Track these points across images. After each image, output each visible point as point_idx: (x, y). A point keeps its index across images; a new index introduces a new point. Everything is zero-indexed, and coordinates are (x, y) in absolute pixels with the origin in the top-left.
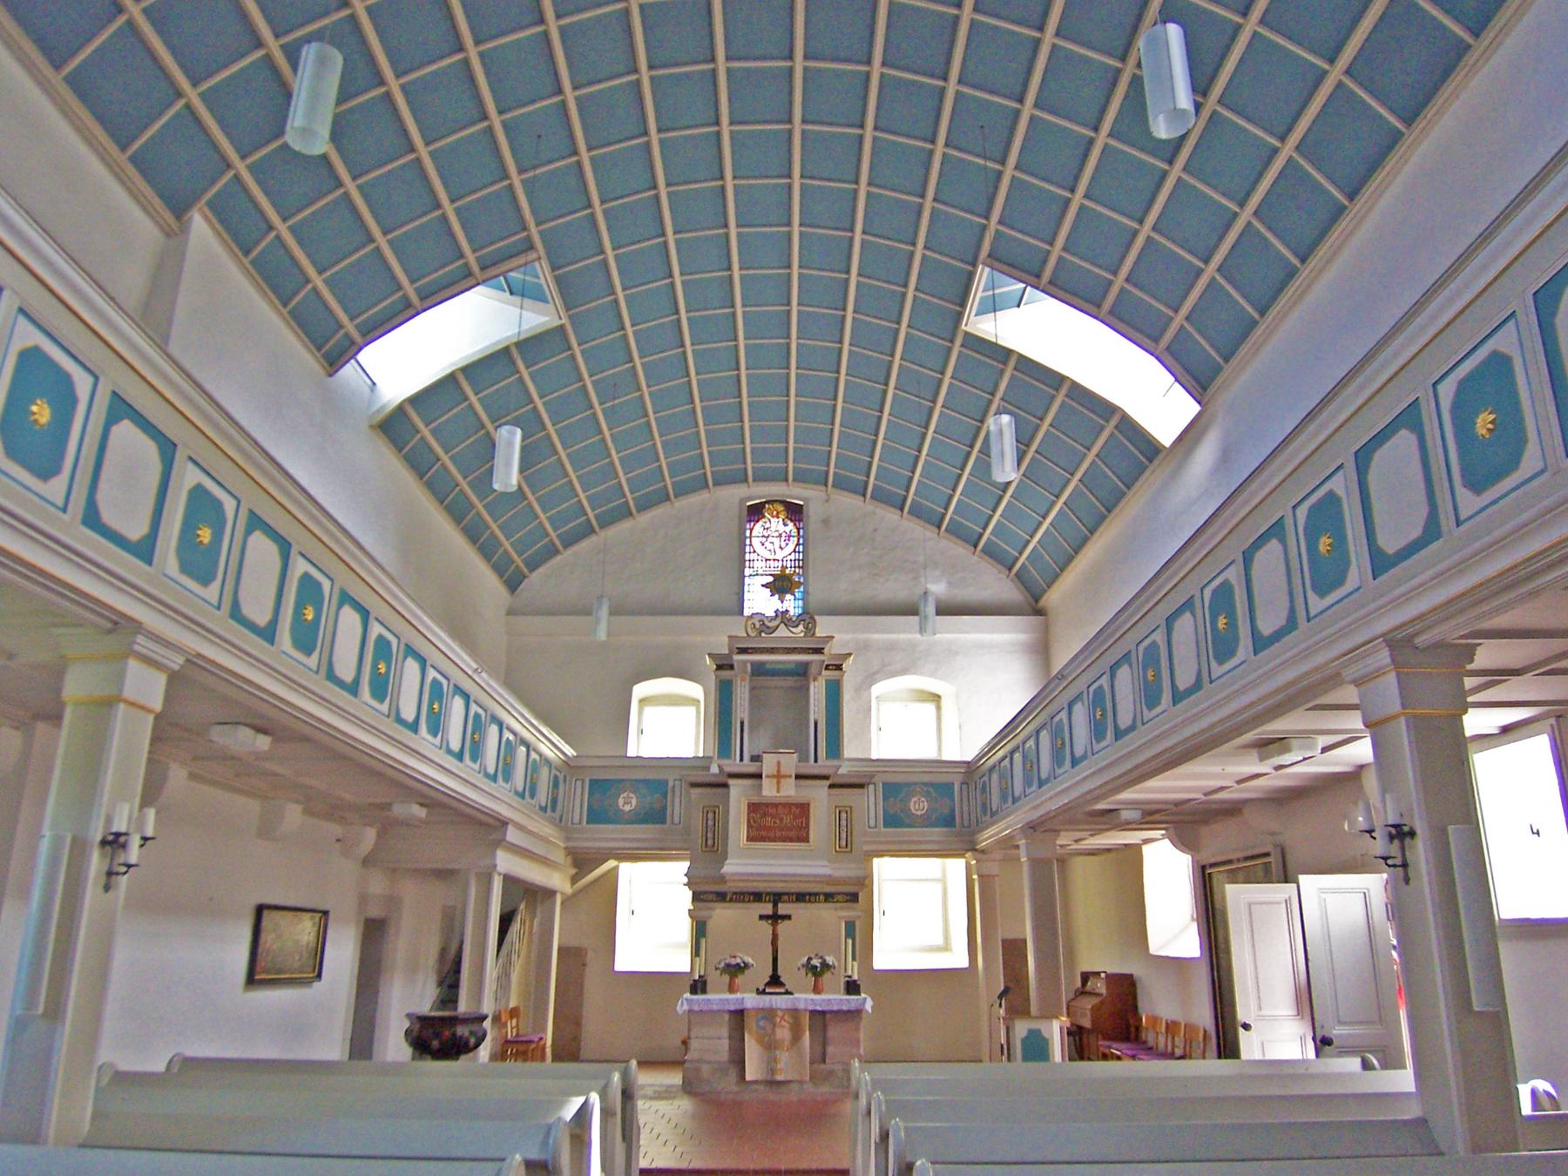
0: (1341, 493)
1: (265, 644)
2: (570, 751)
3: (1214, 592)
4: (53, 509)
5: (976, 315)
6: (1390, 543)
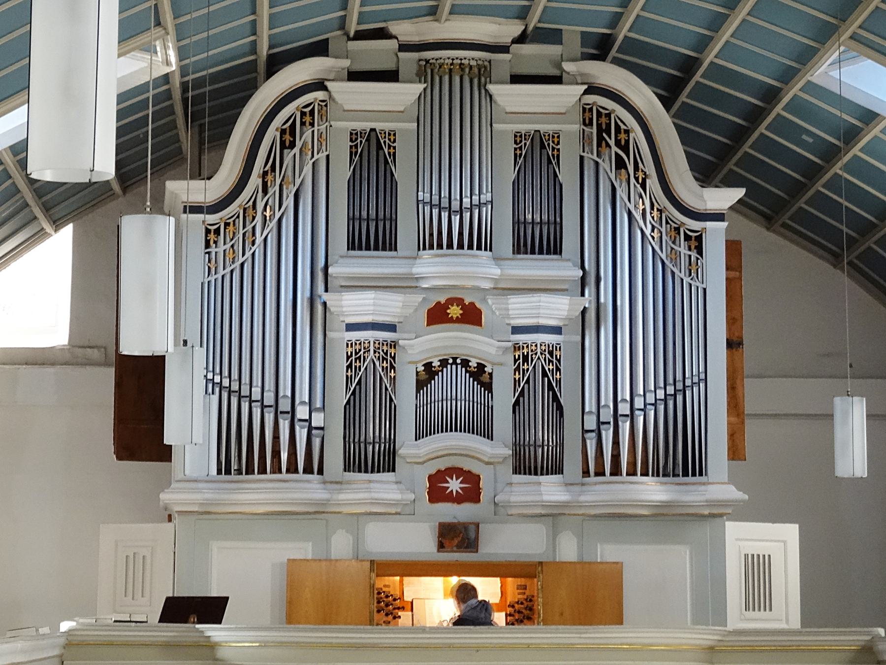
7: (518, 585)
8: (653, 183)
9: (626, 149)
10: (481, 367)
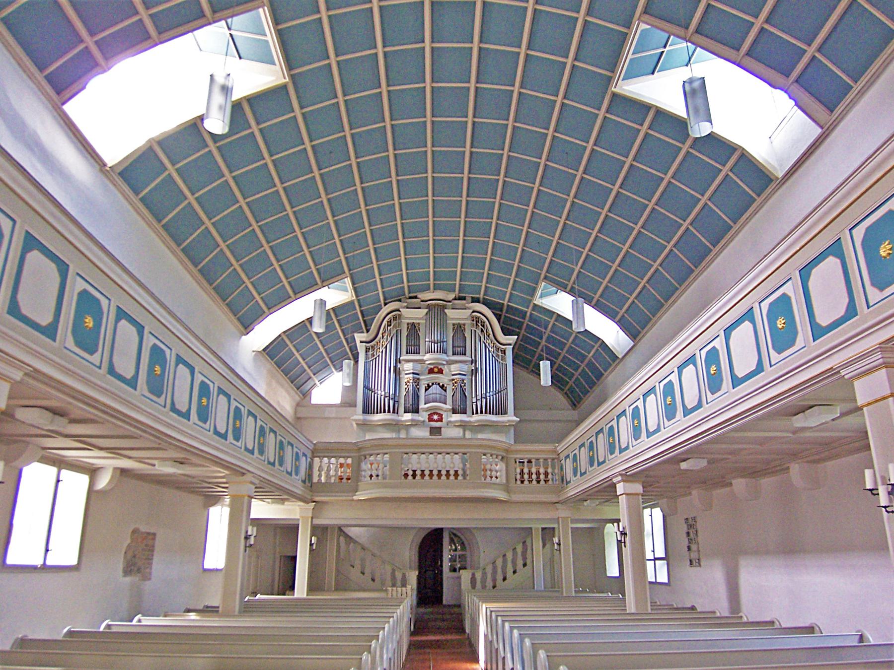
0: (791, 294)
1: (185, 421)
2: (480, 604)
3: (708, 353)
4: (94, 367)
5: (623, 80)
6: (823, 320)
7: (150, 579)
8: (491, 336)
9: (483, 326)
10: (443, 385)
